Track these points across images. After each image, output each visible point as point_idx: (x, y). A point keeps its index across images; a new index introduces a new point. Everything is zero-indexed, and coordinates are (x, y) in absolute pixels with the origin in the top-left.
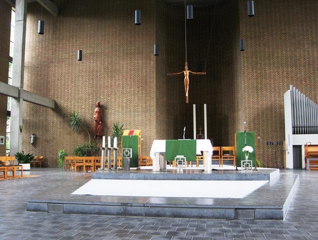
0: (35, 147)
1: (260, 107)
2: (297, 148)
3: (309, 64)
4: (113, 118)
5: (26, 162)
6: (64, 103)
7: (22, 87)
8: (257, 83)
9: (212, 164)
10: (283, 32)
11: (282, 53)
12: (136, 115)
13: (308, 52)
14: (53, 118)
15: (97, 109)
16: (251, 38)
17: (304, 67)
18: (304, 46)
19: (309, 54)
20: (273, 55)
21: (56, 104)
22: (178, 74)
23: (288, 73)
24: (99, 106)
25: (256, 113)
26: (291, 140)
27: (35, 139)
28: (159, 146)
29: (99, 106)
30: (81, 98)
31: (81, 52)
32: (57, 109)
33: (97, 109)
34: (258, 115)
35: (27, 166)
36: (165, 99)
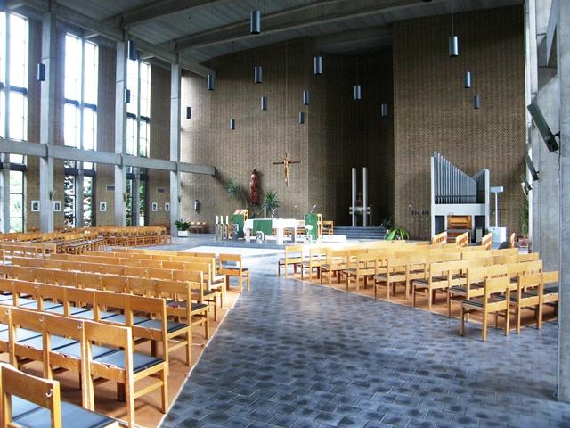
0: (199, 213)
1: (412, 173)
2: (440, 219)
3: (467, 125)
4: (269, 184)
5: (184, 230)
6: (224, 170)
7: (179, 159)
8: (410, 147)
9: (476, 216)
10: (440, 88)
11: (437, 112)
12: (292, 181)
13: (466, 110)
14: (215, 186)
15: (253, 176)
16: (405, 97)
17: (462, 127)
18: (461, 103)
19: (467, 113)
20: (428, 116)
21: (216, 171)
22: (41, 268)
23: (443, 135)
24: (255, 172)
25: (407, 179)
26: (437, 210)
27: (198, 205)
28: (249, 224)
29: (255, 172)
30: (239, 165)
31: (233, 121)
32: (217, 176)
33: (253, 176)
34: (410, 182)
35: (185, 233)
36: (325, 163)
